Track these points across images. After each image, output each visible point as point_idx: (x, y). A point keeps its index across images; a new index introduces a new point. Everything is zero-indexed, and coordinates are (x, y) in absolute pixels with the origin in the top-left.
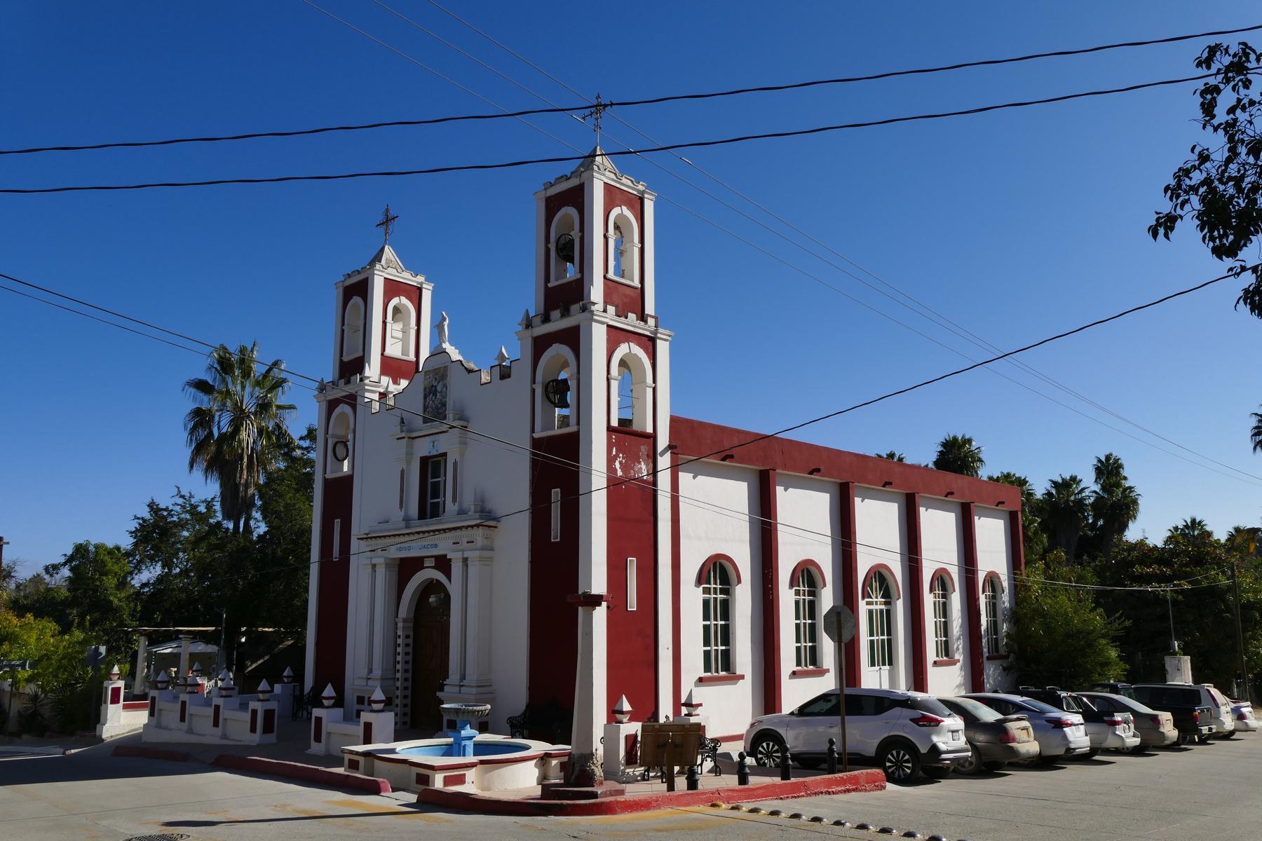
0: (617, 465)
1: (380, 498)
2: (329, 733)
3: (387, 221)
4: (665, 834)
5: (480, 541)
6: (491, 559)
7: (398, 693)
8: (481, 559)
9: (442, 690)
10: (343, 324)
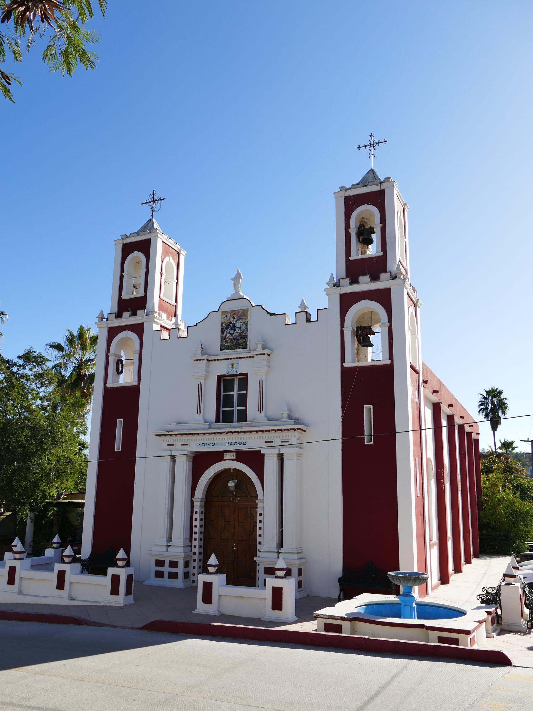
2: (21, 578)
4: (114, 624)
7: (196, 557)
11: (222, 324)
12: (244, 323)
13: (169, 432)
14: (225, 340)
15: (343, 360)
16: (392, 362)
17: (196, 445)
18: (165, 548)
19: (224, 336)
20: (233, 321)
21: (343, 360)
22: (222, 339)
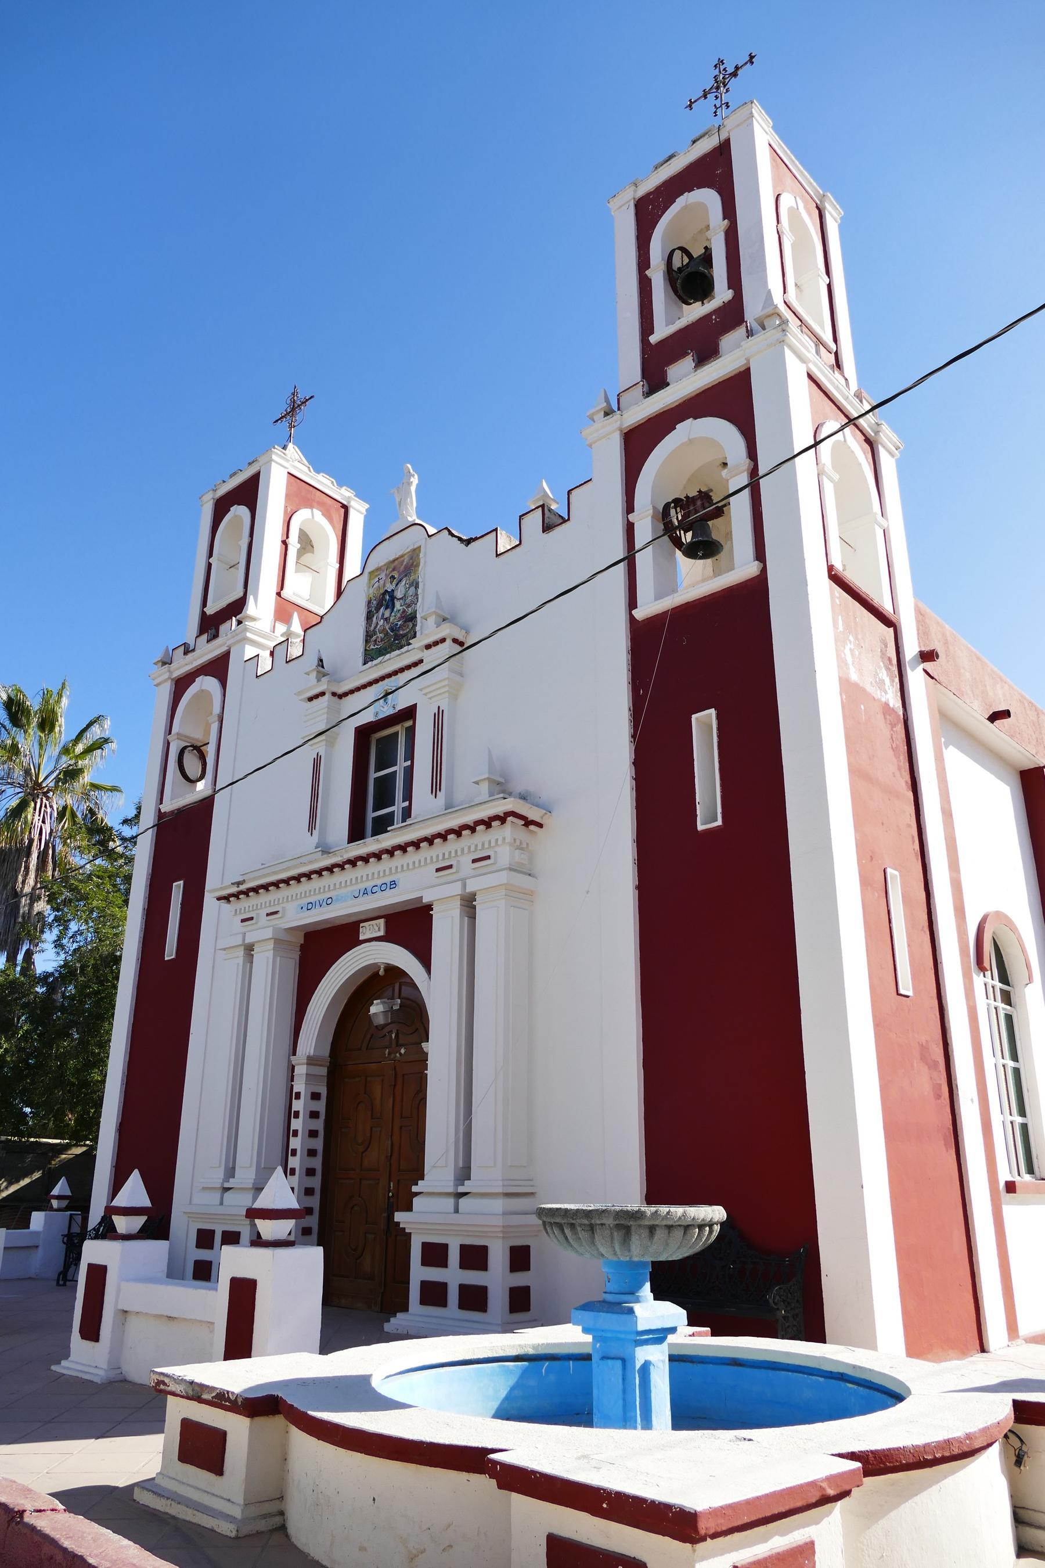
0: (847, 651)
1: (271, 820)
3: (294, 407)
5: (504, 855)
6: (529, 895)
8: (512, 892)
9: (409, 1208)
10: (210, 555)
11: (369, 602)
12: (411, 585)
13: (238, 884)
14: (374, 638)
15: (632, 603)
16: (764, 570)
17: (300, 910)
18: (217, 1195)
19: (372, 628)
20: (389, 587)
21: (632, 603)
22: (368, 636)
